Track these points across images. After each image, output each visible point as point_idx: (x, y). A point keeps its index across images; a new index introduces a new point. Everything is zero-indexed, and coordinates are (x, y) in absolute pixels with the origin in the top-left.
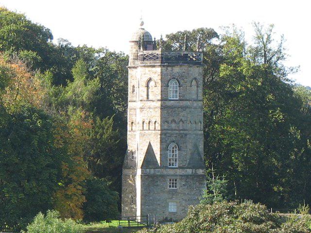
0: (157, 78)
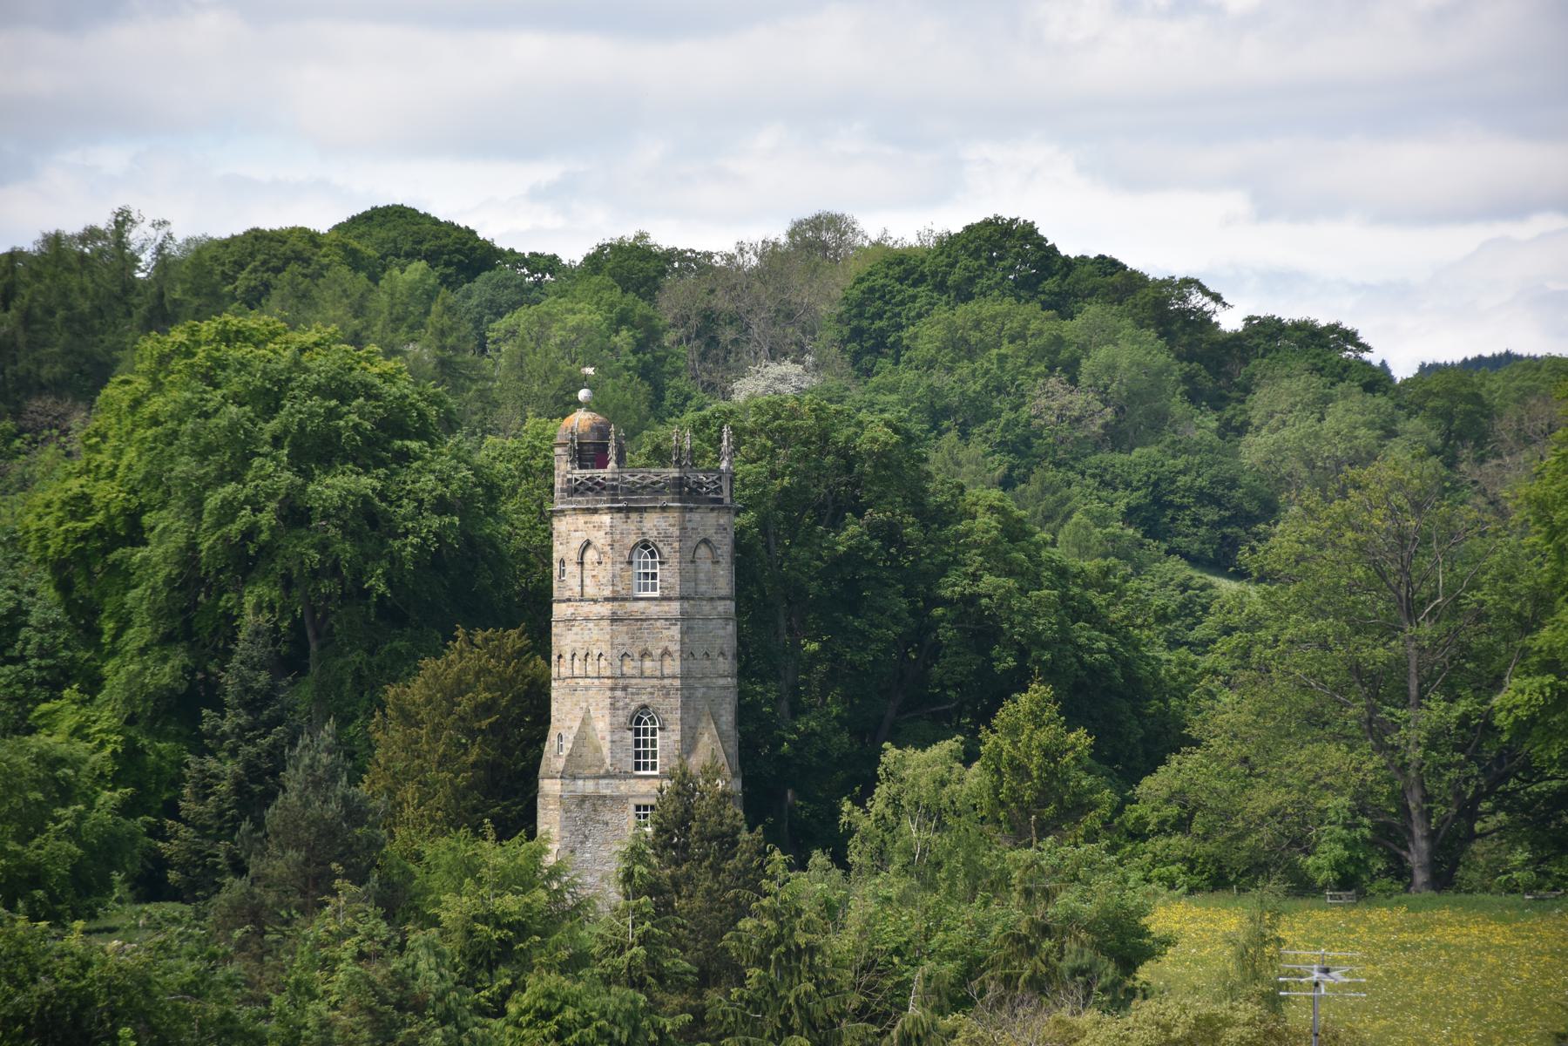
0: (602, 541)
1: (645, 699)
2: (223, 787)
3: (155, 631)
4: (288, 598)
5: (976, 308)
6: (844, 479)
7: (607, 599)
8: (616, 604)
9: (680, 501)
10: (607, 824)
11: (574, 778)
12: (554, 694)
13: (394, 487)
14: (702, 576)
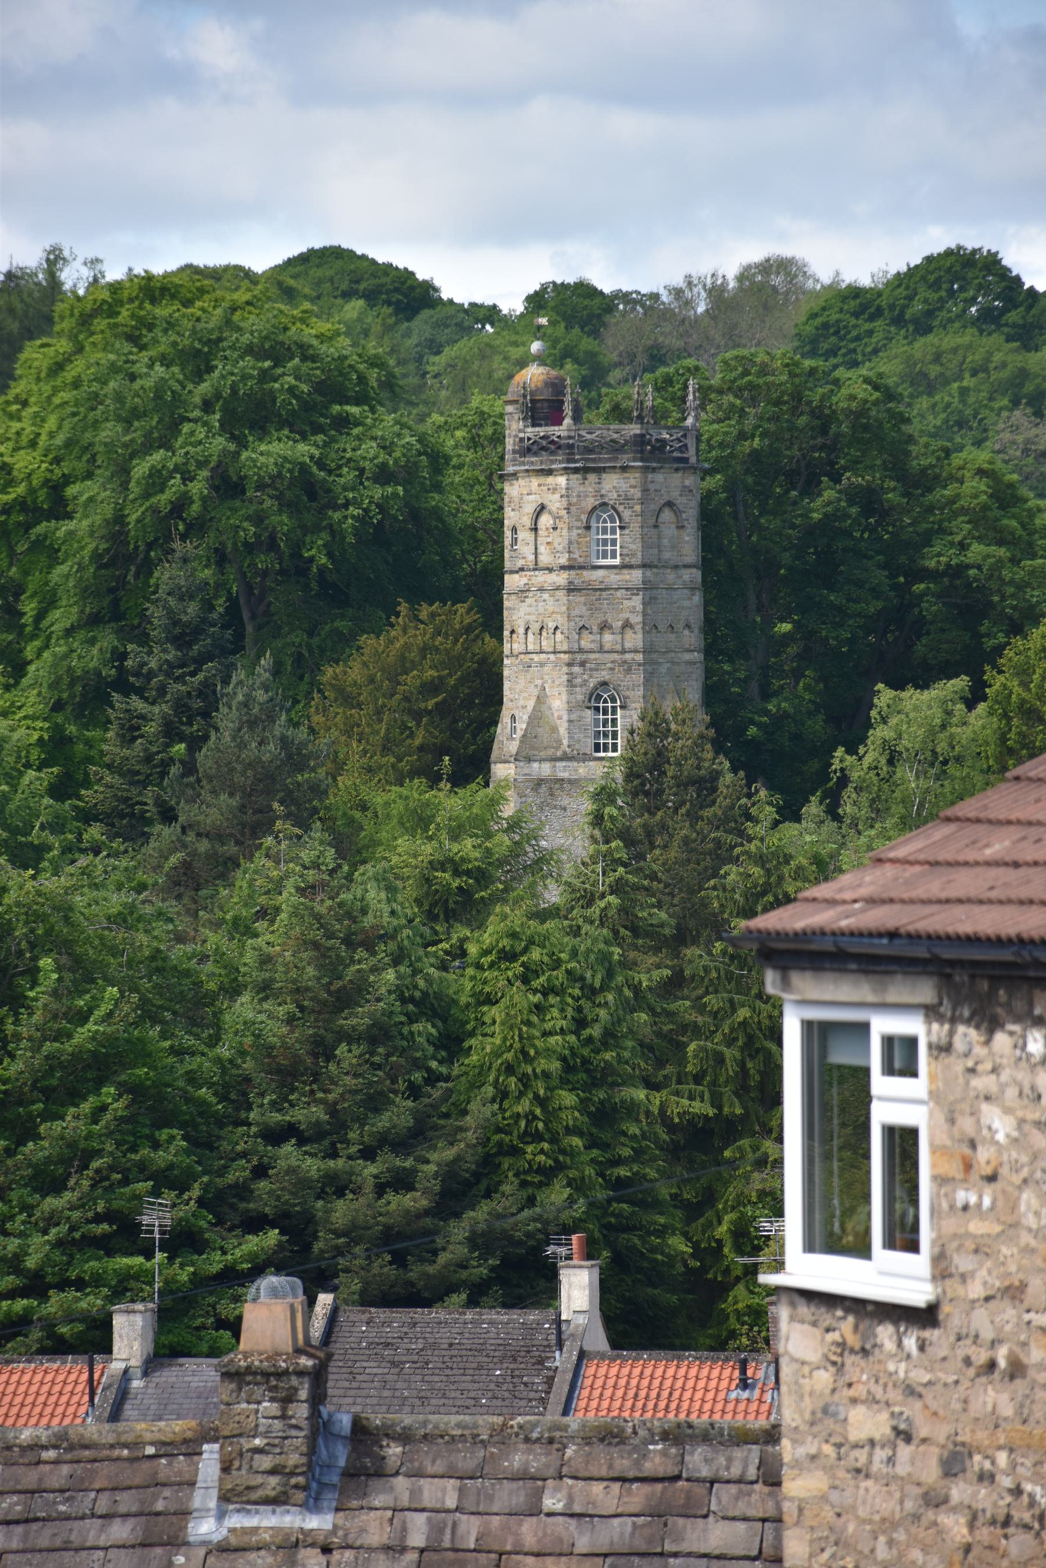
0: (558, 505)
1: (604, 675)
2: (151, 729)
3: (82, 612)
4: (223, 574)
5: (936, 341)
6: (820, 440)
7: (563, 568)
8: (572, 572)
9: (642, 460)
10: (565, 809)
11: (529, 760)
12: (506, 673)
13: (333, 455)
14: (665, 542)
